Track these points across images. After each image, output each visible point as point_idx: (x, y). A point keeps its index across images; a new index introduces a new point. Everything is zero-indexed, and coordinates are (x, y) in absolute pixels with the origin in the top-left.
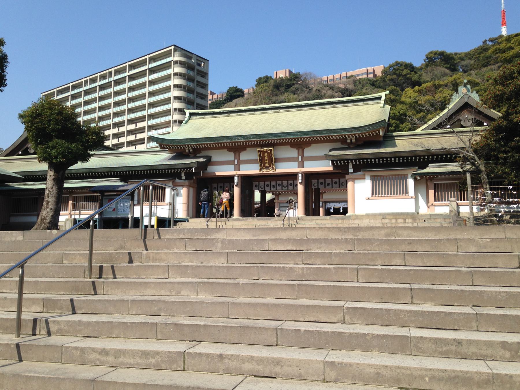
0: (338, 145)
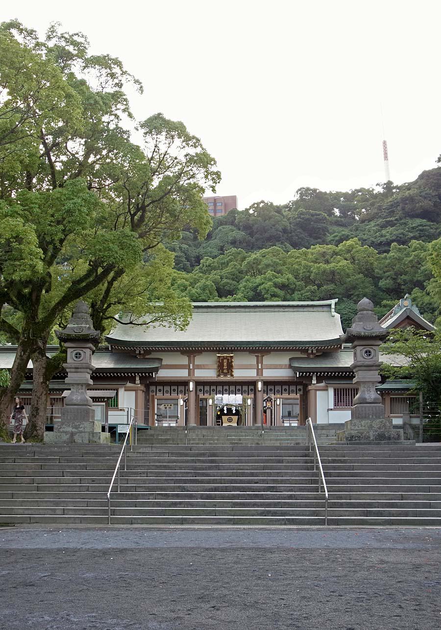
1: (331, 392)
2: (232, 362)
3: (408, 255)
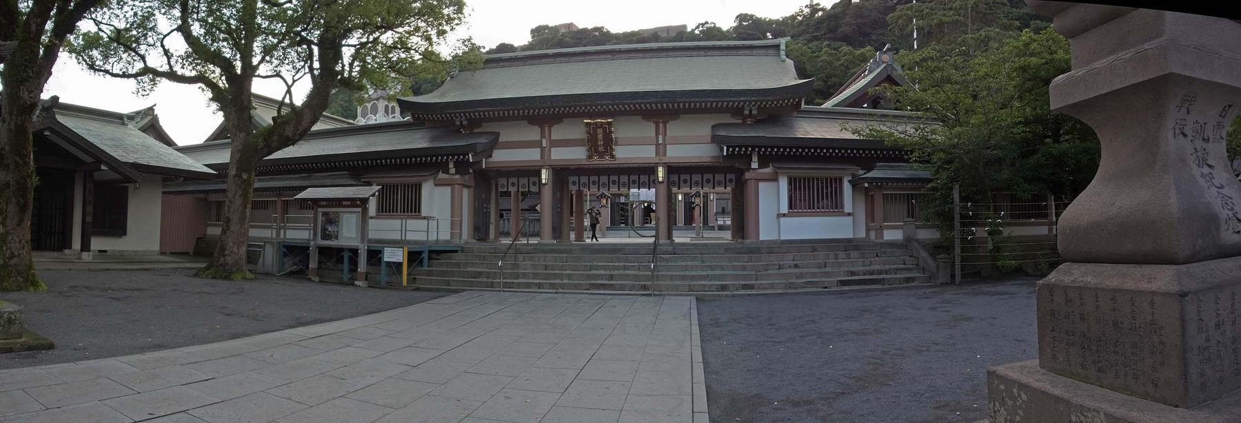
0: (727, 119)
1: (783, 184)
2: (611, 132)
3: (838, 60)
